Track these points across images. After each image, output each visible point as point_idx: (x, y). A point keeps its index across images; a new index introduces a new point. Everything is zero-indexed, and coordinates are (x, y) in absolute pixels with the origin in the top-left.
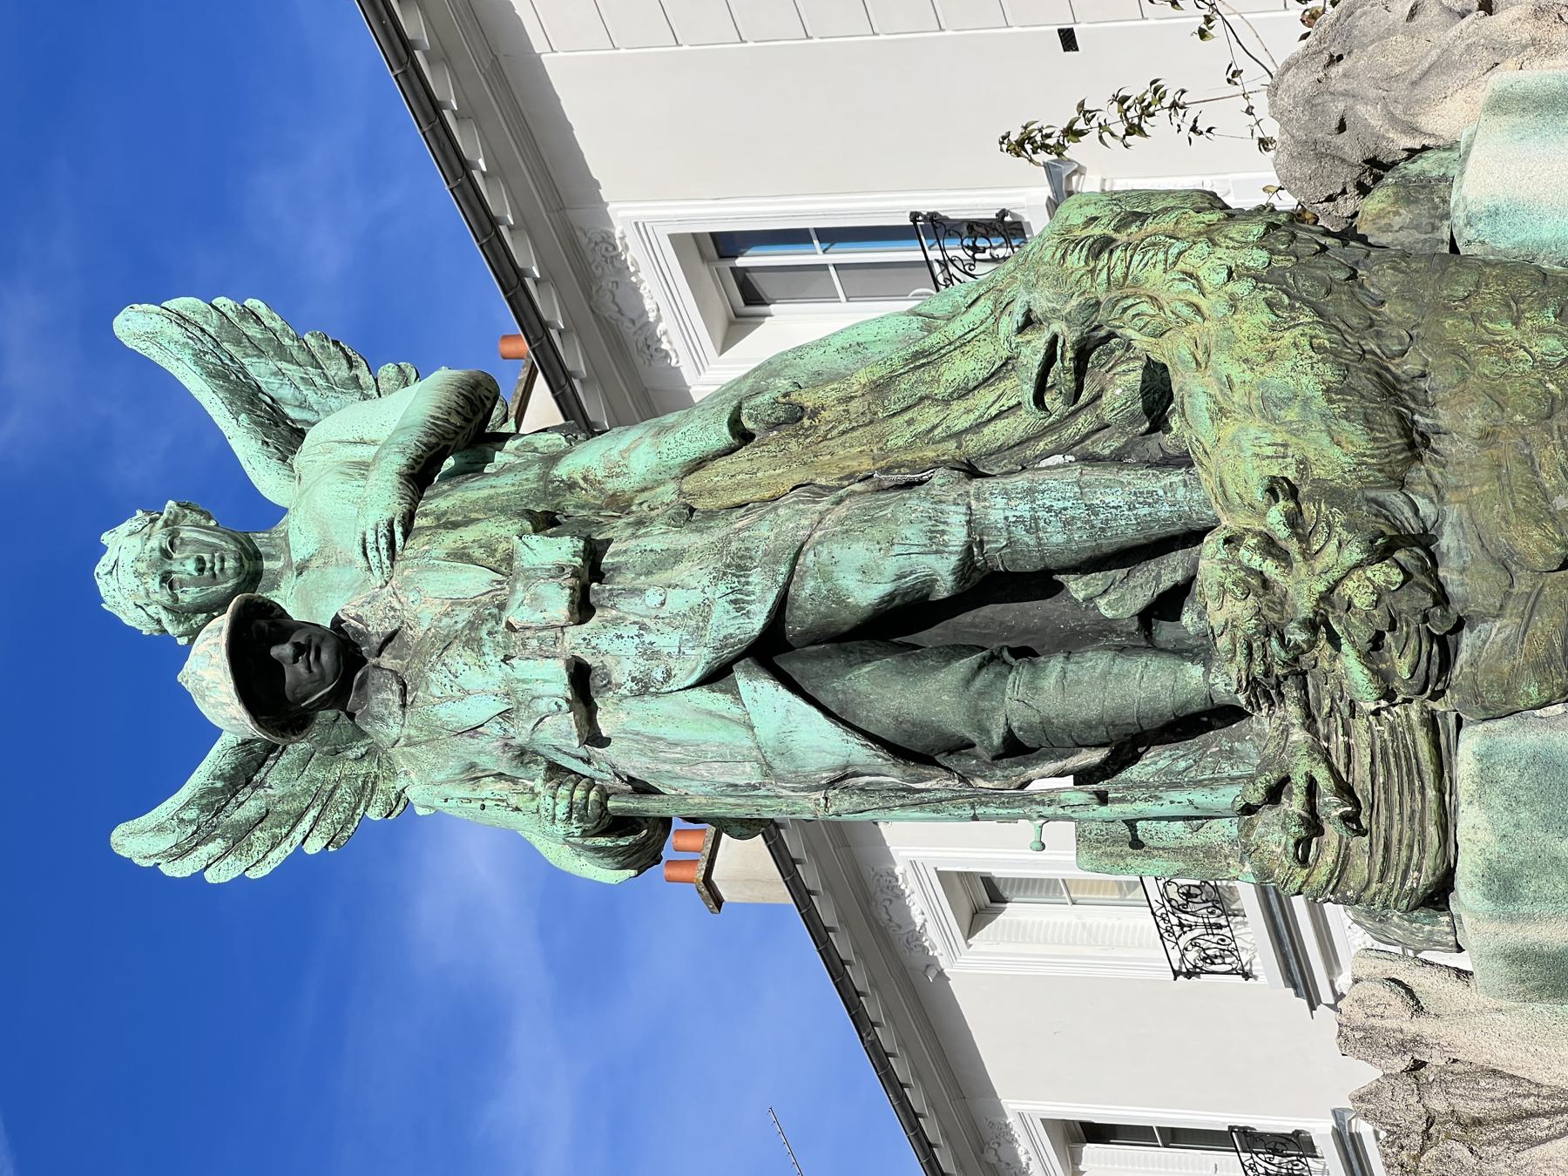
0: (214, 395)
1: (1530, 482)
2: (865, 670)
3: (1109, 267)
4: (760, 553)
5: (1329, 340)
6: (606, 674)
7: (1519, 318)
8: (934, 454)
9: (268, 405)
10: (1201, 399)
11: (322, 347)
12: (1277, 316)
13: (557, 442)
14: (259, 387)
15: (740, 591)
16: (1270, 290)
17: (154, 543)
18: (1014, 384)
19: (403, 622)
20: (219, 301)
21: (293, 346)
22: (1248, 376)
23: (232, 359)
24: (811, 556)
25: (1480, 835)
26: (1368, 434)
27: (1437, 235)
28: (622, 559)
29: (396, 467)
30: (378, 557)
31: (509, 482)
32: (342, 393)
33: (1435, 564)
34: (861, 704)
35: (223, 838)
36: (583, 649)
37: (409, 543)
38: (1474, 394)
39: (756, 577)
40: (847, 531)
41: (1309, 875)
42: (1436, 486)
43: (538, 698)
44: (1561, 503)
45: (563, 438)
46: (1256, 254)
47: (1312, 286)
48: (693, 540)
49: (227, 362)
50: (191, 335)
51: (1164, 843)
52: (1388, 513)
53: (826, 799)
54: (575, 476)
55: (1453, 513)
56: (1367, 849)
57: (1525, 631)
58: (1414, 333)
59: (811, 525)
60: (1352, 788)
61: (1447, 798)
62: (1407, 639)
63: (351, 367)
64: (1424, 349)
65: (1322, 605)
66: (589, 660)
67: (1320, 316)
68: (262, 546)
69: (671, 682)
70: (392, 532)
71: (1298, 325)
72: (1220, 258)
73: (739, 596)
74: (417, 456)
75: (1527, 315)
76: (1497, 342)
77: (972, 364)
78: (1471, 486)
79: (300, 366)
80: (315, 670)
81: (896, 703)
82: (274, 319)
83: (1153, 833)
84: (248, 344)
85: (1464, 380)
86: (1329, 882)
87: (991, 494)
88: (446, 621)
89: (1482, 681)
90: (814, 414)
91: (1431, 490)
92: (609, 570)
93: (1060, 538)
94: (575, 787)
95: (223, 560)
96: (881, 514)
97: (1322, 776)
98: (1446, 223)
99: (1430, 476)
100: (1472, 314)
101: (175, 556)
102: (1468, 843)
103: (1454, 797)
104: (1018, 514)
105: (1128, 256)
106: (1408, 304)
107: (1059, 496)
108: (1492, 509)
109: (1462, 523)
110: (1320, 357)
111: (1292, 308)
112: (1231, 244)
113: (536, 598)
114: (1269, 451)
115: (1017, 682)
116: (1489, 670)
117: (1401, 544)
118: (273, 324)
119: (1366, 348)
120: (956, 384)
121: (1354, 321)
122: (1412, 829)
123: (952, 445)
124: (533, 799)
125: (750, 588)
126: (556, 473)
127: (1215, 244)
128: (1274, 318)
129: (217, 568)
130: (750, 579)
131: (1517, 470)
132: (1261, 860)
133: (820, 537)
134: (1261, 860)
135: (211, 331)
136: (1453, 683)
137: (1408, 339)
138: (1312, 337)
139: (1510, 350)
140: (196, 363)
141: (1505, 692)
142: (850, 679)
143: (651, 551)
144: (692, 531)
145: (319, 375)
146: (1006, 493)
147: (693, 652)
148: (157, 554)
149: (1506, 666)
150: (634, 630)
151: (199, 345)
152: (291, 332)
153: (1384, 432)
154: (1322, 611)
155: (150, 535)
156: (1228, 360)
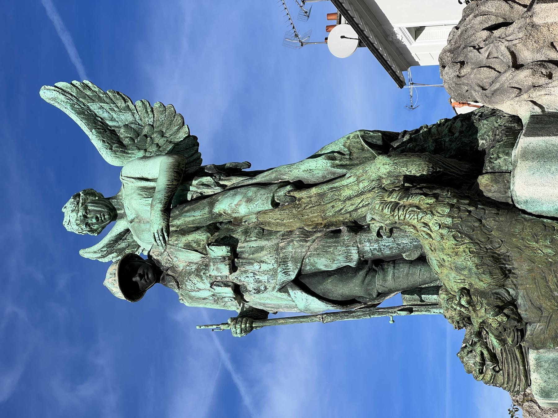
0: (81, 122)
1: (545, 286)
2: (329, 281)
3: (398, 216)
4: (290, 256)
5: (475, 249)
6: (245, 287)
7: (538, 241)
8: (342, 219)
9: (100, 122)
10: (434, 262)
11: (114, 96)
12: (457, 241)
13: (210, 180)
14: (96, 114)
15: (286, 269)
16: (454, 232)
17: (80, 214)
18: (367, 197)
19: (173, 265)
20: (74, 82)
21: (104, 97)
22: (450, 259)
23: (84, 105)
24: (307, 260)
25: (538, 381)
26: (491, 278)
27: (507, 195)
28: (243, 250)
29: (159, 209)
30: (160, 243)
31: (199, 214)
32: (125, 113)
33: (517, 308)
34: (330, 292)
35: (116, 252)
36: (236, 281)
37: (170, 239)
38: (525, 259)
39: (290, 264)
40: (318, 254)
41: (484, 376)
42: (515, 285)
43: (224, 298)
44: (556, 294)
45: (211, 179)
46: (448, 219)
47: (468, 229)
48: (266, 243)
49: (83, 106)
50: (68, 98)
51: (431, 301)
52: (500, 296)
53: (322, 318)
54: (221, 212)
55: (521, 293)
56: (502, 374)
57: (548, 327)
58: (503, 240)
59: (306, 251)
60: (495, 354)
61: (526, 367)
62: (510, 333)
63: (125, 102)
64: (507, 246)
65: (481, 324)
66: (239, 284)
67: (471, 240)
68: (115, 206)
69: (267, 290)
70: (163, 233)
71: (464, 243)
72: (436, 220)
73: (285, 270)
74: (166, 202)
75: (540, 241)
76: (531, 247)
77: (351, 192)
78: (526, 284)
79: (108, 104)
80: (148, 281)
81: (341, 291)
82: (95, 88)
83: (427, 298)
84: (88, 98)
85: (521, 255)
86: (490, 380)
87: (365, 241)
88: (188, 268)
89: (535, 340)
90: (300, 200)
91: (513, 286)
92: (240, 253)
93: (389, 252)
94: (241, 323)
95: (104, 216)
96: (329, 250)
97: (485, 353)
98: (509, 190)
99: (512, 282)
100: (522, 238)
101: (88, 216)
102: (534, 383)
103: (528, 366)
104: (374, 248)
105: (404, 213)
106: (500, 232)
107: (387, 242)
108: (534, 294)
109: (524, 296)
110: (473, 255)
111: (462, 237)
112: (439, 215)
113: (218, 269)
114: (459, 281)
115: (379, 278)
116: (537, 337)
117: (505, 307)
118: (95, 89)
119: (487, 248)
120: (347, 197)
121: (483, 240)
122: (516, 372)
123: (348, 215)
124: (229, 327)
125: (289, 267)
126: (214, 211)
127: (434, 215)
128: (456, 242)
129: (103, 219)
130: (288, 265)
131: (541, 281)
132: (468, 368)
133: (309, 254)
134: (468, 368)
135: (74, 94)
136: (526, 340)
137: (501, 243)
138: (469, 248)
139: (536, 250)
140: (72, 109)
141: (542, 344)
142: (325, 285)
143: (253, 247)
144: (265, 240)
145: (115, 107)
146: (369, 241)
147: (273, 281)
148: (82, 218)
149: (542, 337)
150: (252, 275)
151: (72, 102)
152: (102, 91)
153: (496, 275)
154: (482, 326)
155: (78, 210)
156: (442, 254)
